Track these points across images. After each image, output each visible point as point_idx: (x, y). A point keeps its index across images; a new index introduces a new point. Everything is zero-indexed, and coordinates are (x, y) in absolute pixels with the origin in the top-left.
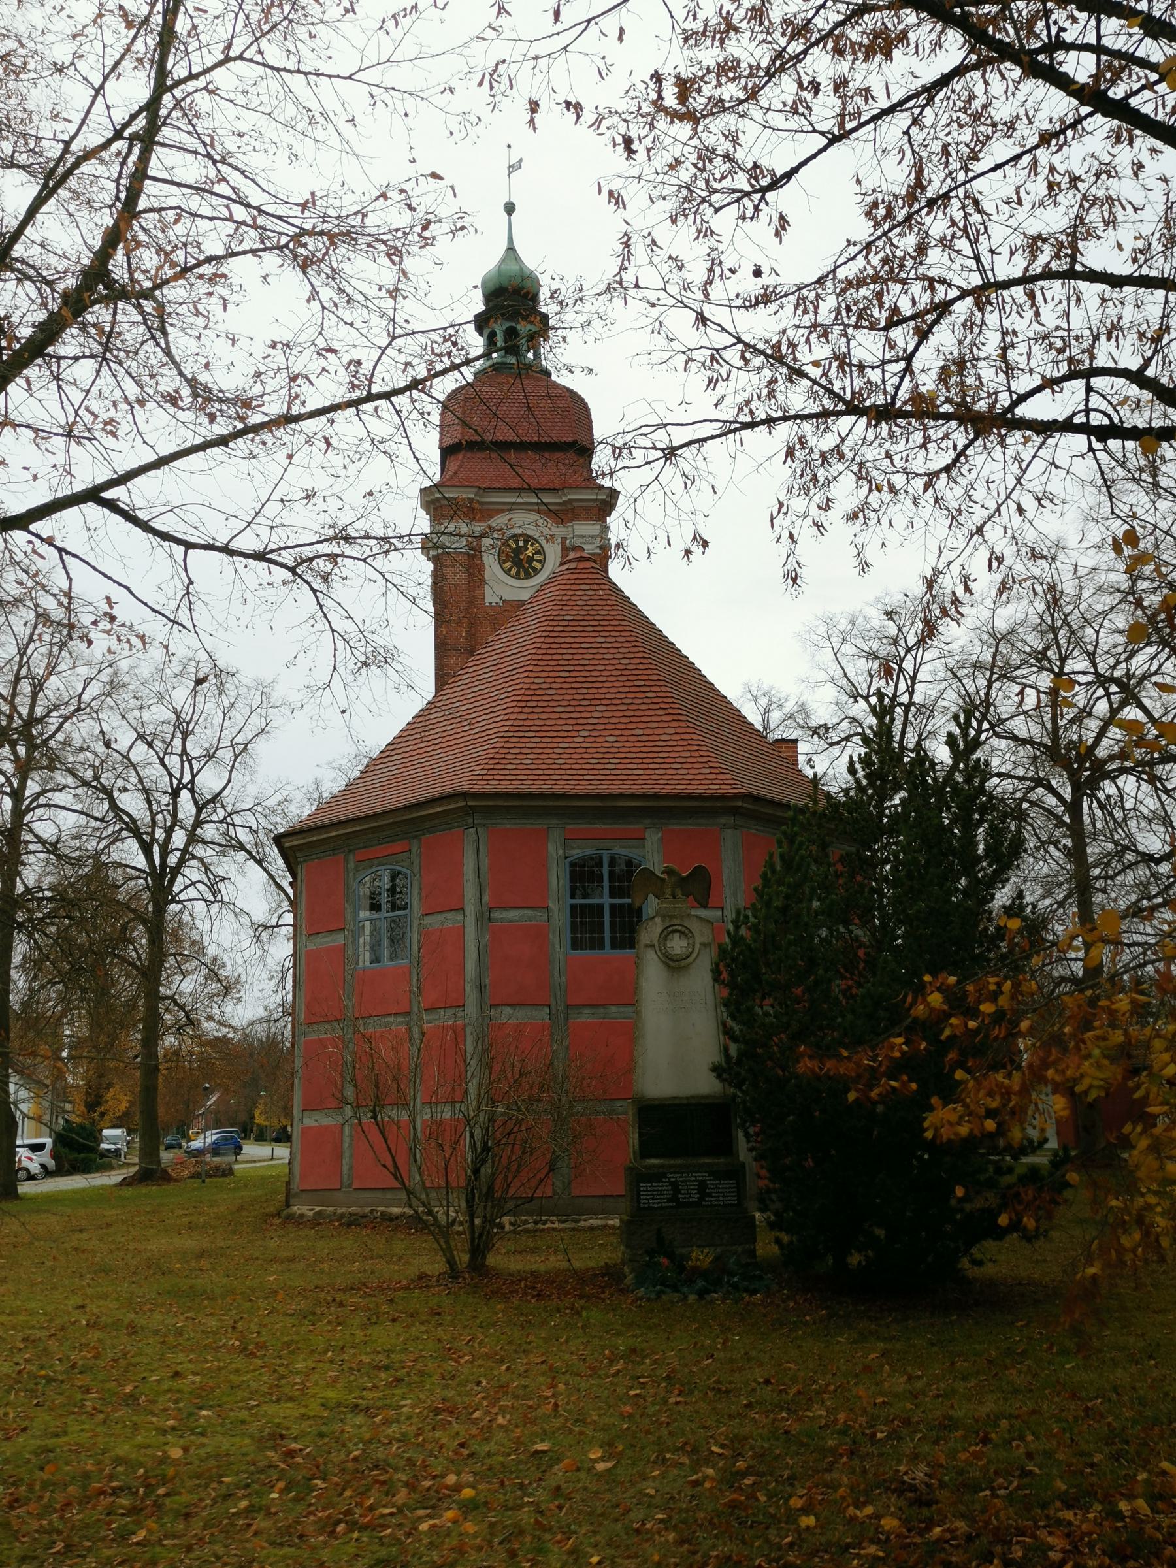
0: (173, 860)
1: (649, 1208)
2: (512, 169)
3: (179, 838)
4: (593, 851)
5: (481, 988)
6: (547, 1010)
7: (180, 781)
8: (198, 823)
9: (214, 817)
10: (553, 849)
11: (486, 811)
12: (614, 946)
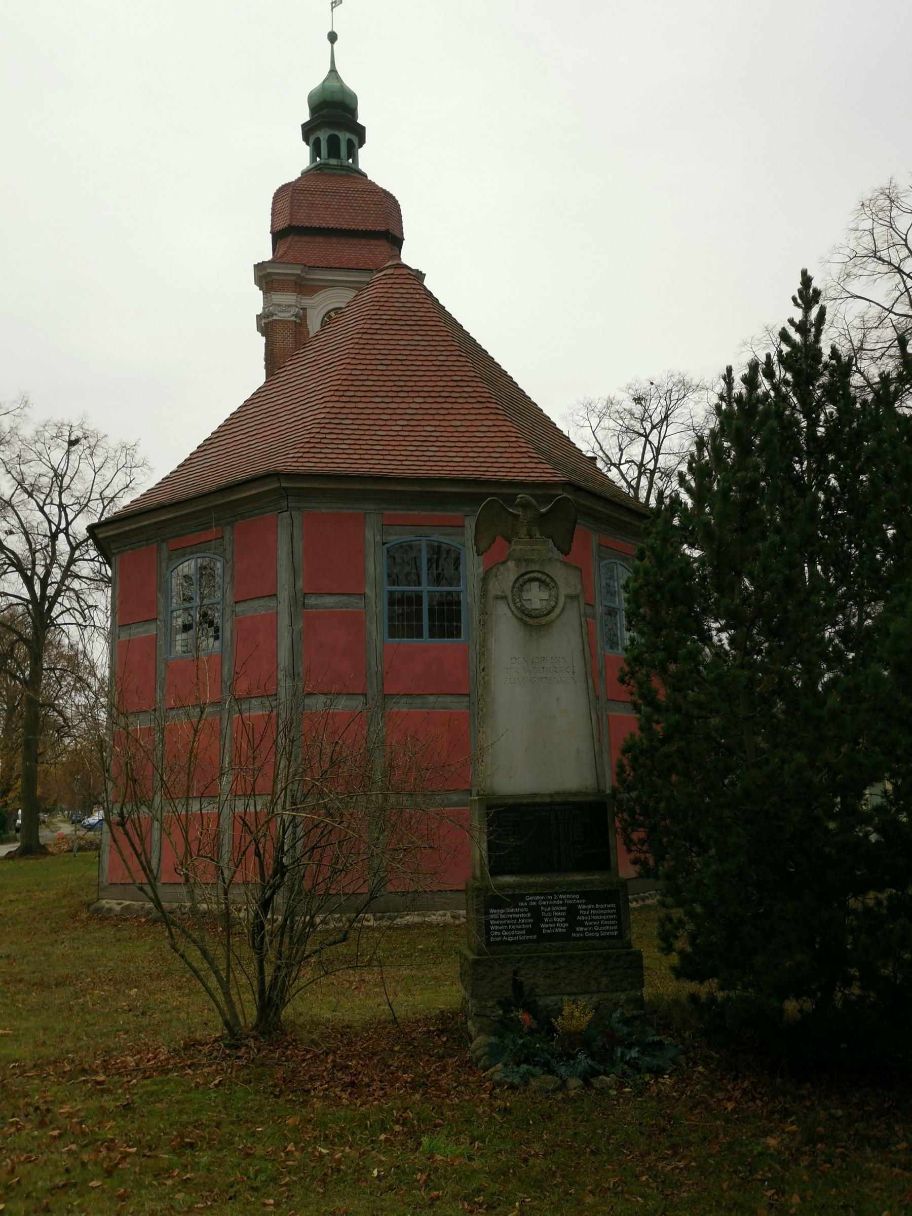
0: (50, 591)
1: (502, 943)
3: (56, 574)
4: (412, 538)
6: (361, 698)
7: (58, 526)
8: (72, 561)
9: (87, 557)
10: (371, 535)
11: (303, 494)
12: (432, 635)
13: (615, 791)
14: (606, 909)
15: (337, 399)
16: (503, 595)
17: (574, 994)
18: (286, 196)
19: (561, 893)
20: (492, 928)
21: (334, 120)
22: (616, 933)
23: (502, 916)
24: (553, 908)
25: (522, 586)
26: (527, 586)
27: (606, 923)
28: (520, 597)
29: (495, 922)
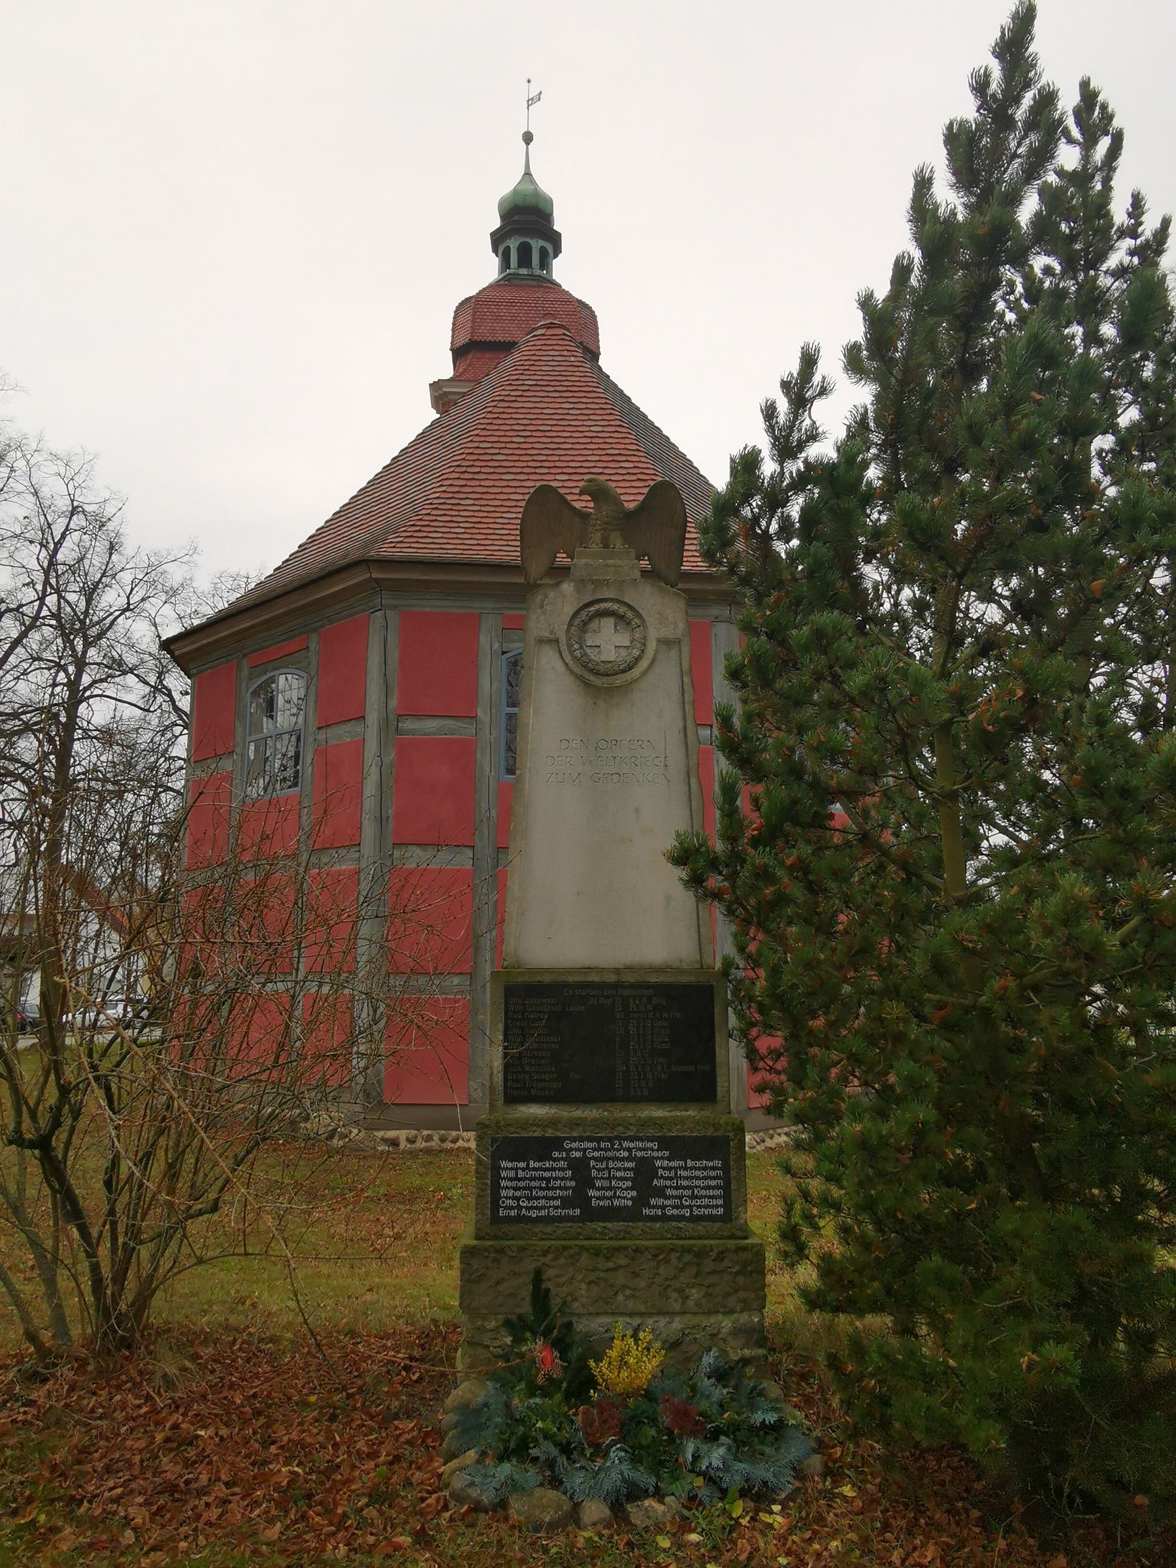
1: (519, 1219)
2: (531, 102)
5: (381, 820)
6: (470, 853)
11: (401, 588)
13: (728, 964)
14: (705, 1168)
15: (457, 475)
16: (552, 637)
17: (641, 1314)
18: (472, 310)
19: (626, 1139)
20: (503, 1193)
21: (527, 228)
22: (721, 1211)
23: (521, 1174)
24: (611, 1164)
25: (585, 623)
26: (594, 625)
27: (703, 1192)
28: (581, 641)
29: (510, 1184)
